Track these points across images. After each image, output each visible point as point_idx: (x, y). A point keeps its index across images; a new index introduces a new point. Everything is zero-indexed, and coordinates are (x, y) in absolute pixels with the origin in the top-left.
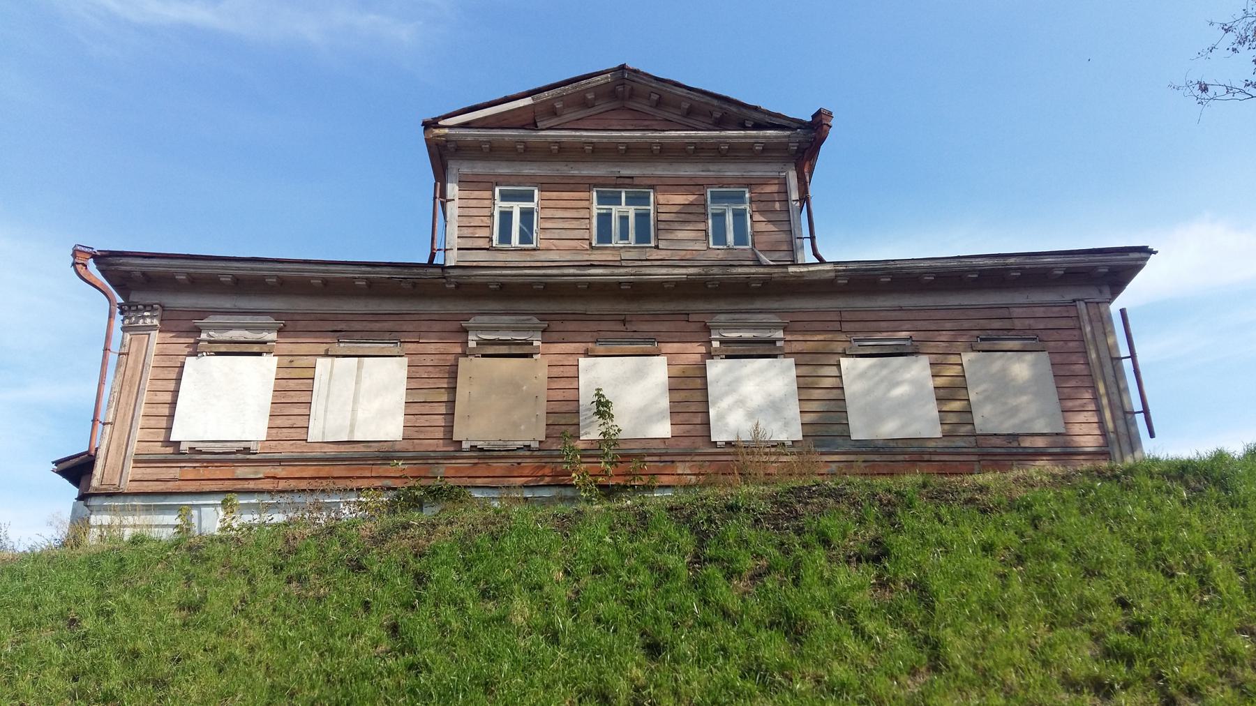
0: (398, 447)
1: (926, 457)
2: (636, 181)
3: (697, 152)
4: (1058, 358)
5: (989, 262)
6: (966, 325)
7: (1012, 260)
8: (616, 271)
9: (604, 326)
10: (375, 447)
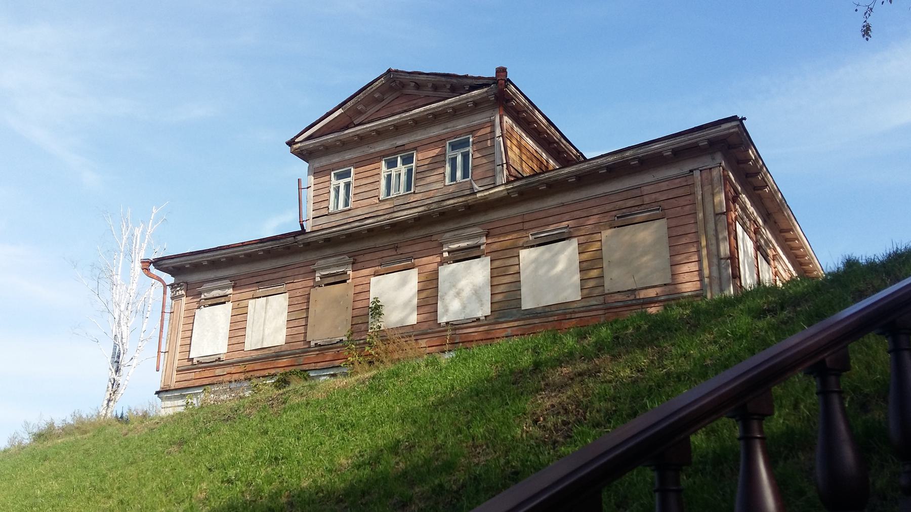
0: (283, 349)
1: (568, 316)
2: (407, 147)
3: (436, 118)
4: (674, 223)
5: (611, 159)
6: (608, 208)
7: (628, 154)
8: (379, 219)
9: (385, 253)
10: (273, 350)
